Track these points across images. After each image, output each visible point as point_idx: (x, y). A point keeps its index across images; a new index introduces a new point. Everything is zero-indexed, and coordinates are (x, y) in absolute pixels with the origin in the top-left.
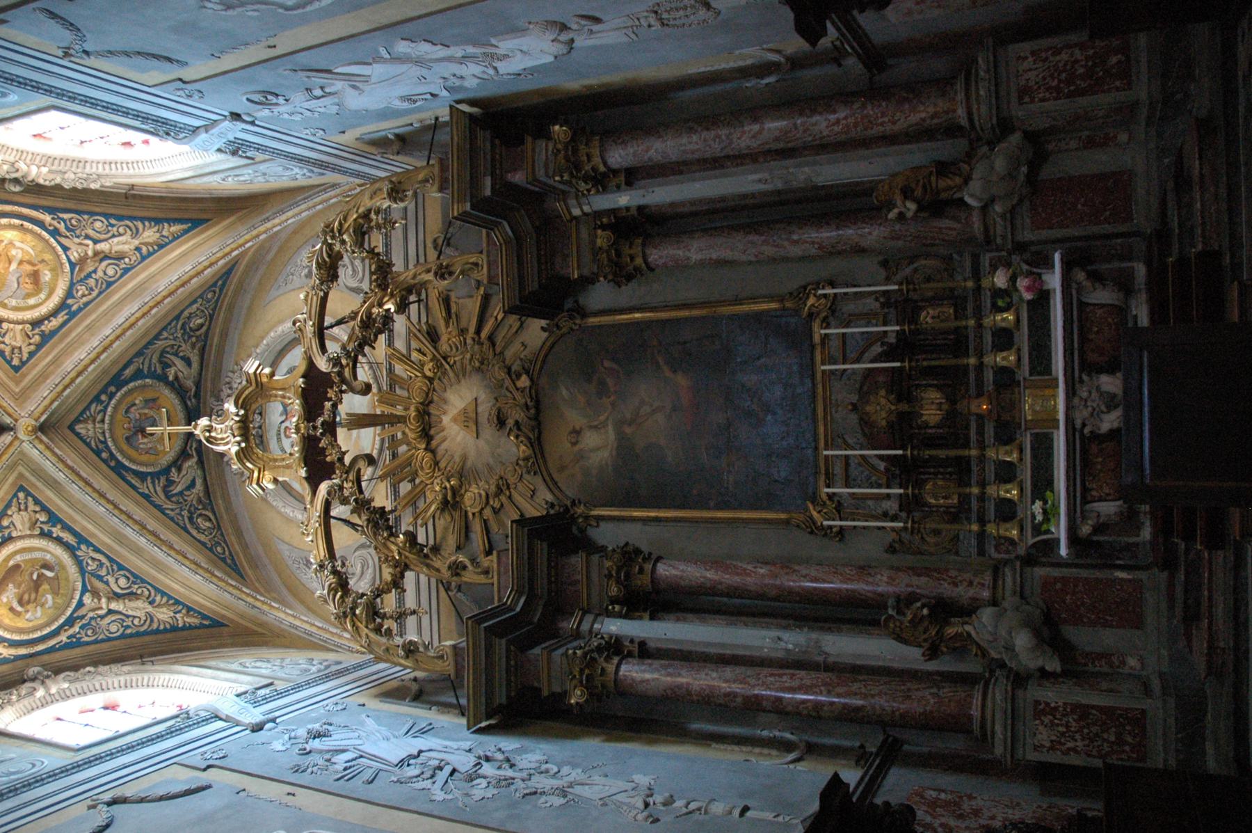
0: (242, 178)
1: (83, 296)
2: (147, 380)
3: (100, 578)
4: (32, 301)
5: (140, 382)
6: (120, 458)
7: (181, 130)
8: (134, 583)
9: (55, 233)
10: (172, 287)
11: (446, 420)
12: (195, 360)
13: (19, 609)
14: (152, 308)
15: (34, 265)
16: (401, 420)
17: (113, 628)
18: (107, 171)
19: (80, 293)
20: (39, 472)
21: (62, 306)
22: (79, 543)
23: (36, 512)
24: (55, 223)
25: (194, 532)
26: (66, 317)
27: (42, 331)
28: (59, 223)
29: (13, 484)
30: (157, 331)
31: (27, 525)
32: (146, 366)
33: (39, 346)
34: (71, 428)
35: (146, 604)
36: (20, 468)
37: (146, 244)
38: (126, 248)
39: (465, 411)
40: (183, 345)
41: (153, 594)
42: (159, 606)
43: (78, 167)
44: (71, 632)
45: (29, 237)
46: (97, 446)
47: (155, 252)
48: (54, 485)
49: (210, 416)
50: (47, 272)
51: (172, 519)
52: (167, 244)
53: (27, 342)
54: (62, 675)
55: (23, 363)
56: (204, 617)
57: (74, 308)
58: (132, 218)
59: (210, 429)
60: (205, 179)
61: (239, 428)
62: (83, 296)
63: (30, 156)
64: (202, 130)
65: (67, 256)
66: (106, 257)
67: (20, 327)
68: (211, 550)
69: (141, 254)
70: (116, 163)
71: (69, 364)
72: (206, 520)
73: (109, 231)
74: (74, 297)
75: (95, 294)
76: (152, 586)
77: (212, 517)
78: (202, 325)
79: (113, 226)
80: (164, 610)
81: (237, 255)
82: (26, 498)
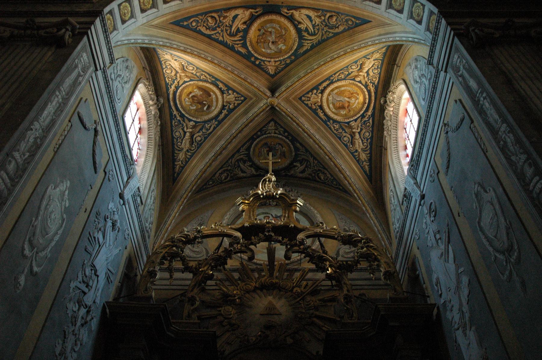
0: (392, 199)
1: (334, 127)
2: (294, 153)
3: (201, 129)
4: (331, 106)
5: (293, 150)
9: (363, 116)
10: (339, 166)
11: (270, 298)
12: (304, 175)
13: (191, 96)
14: (328, 156)
15: (348, 107)
16: (271, 275)
17: (177, 134)
18: (392, 139)
19: (335, 126)
22: (218, 121)
23: (234, 104)
24: (367, 116)
25: (220, 172)
26: (324, 119)
28: (368, 118)
29: (248, 96)
31: (228, 100)
32: (301, 153)
33: (310, 108)
34: (272, 120)
35: (187, 148)
36: (255, 98)
38: (357, 146)
39: (275, 308)
40: (311, 170)
41: (192, 152)
42: (186, 154)
43: (393, 126)
44: (177, 116)
45: (360, 106)
46: (263, 130)
47: (355, 158)
48: (246, 112)
49: (276, 182)
50: (345, 112)
51: (227, 161)
52: (359, 164)
54: (158, 112)
55: (303, 101)
56: (178, 174)
57: (328, 123)
59: (270, 181)
60: (391, 182)
61: (270, 195)
62: (334, 127)
63: (397, 108)
65: (352, 121)
66: (352, 137)
67: (319, 101)
68: (211, 179)
71: (302, 120)
73: (364, 139)
74: (333, 123)
75: (335, 132)
76: (195, 152)
78: (320, 179)
79: (367, 140)
80: (184, 156)
82: (241, 100)
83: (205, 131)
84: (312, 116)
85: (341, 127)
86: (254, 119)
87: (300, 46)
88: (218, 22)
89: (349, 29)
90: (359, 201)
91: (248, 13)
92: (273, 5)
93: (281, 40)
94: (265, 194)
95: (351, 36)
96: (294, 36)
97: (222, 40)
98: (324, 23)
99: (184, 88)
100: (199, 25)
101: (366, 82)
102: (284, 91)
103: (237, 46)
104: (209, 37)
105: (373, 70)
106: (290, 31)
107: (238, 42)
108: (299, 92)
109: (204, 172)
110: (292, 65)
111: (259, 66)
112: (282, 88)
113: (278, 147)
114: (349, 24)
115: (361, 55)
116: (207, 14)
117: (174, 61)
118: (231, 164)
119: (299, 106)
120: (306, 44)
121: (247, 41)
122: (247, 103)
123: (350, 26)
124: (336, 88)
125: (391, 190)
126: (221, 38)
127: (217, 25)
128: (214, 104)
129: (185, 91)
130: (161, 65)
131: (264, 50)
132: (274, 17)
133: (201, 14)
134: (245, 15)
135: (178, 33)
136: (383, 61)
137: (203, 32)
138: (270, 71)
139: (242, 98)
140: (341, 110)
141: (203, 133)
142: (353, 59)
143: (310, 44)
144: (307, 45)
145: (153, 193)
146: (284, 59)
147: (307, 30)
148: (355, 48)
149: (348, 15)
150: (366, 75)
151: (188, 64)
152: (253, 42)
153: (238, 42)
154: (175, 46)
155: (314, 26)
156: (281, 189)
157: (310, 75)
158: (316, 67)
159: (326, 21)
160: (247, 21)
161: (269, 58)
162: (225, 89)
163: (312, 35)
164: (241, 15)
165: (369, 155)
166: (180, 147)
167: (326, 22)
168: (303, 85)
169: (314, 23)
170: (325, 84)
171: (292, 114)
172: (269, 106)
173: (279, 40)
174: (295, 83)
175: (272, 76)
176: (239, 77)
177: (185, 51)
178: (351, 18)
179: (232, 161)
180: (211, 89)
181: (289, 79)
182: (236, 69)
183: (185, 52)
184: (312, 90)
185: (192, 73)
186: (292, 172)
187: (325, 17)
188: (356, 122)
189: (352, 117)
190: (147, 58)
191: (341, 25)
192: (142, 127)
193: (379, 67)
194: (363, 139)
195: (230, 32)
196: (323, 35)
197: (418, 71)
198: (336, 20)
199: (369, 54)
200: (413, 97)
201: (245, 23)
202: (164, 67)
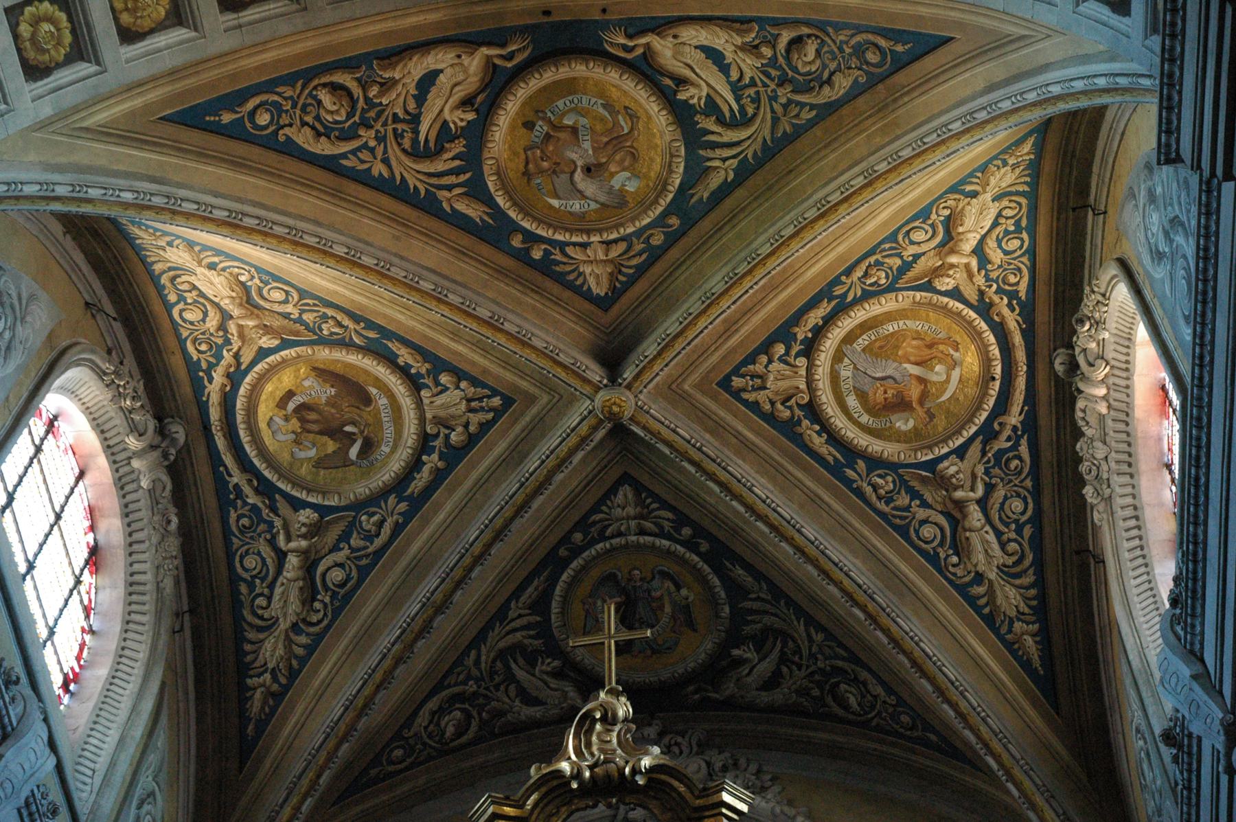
0: (1145, 766)
1: (875, 488)
2: (727, 609)
3: (345, 537)
4: (852, 401)
5: (723, 594)
6: (574, 565)
7: (1190, 629)
8: (334, 595)
9: (988, 433)
10: (909, 644)
12: (777, 696)
13: (291, 406)
14: (864, 609)
15: (921, 402)
17: (250, 562)
18: (1120, 513)
19: (880, 481)
20: (538, 428)
21: (851, 453)
22: (410, 499)
23: (466, 426)
24: (1007, 432)
25: (432, 704)
26: (830, 459)
27: (799, 422)
28: (1009, 439)
29: (516, 388)
30: (824, 621)
31: (442, 413)
32: (756, 605)
33: (770, 418)
34: (625, 479)
35: (292, 618)
36: (545, 398)
37: (991, 592)
40: (803, 673)
41: (312, 630)
42: (289, 642)
43: (1118, 462)
44: (247, 489)
45: (972, 391)
46: (594, 523)
47: (978, 610)
48: (517, 454)
49: (633, 721)
50: (911, 424)
51: (459, 662)
52: (996, 631)
53: (775, 398)
54: (166, 479)
55: (736, 394)
56: (262, 725)
57: (850, 473)
58: (1039, 564)
59: (609, 719)
60: (1132, 693)
61: (608, 776)
62: (875, 488)
63: (1123, 383)
64: (1198, 668)
65: (946, 456)
66: (955, 523)
67: (803, 386)
68: (398, 736)
69: (970, 584)
70: (1139, 528)
71: (741, 468)
72: (457, 727)
73: (1007, 525)
74: (870, 470)
75: (882, 506)
76: (328, 627)
77: (464, 739)
78: (846, 707)
79: (1019, 531)
80: (280, 651)
81: (989, 767)
82: (491, 410)
83: (362, 543)
84: (783, 451)
85: (903, 483)
86: (548, 479)
87: (696, 172)
88: (361, 103)
89: (875, 81)
90: (1010, 786)
91: (474, 63)
92: (571, 23)
93: (618, 157)
94: (587, 774)
95: (882, 109)
96: (668, 138)
97: (386, 175)
98: (774, 73)
99: (263, 378)
100: (285, 120)
101: (981, 293)
102: (655, 358)
103: (446, 194)
104: (329, 164)
105: (999, 241)
106: (649, 118)
107: (452, 180)
108: (714, 358)
109: (366, 706)
110: (674, 253)
111: (545, 267)
112: (645, 345)
113: (661, 588)
114: (868, 63)
115: (937, 183)
116: (311, 80)
117: (206, 272)
118: (475, 672)
119: (722, 413)
120: (717, 163)
121: (486, 170)
122: (516, 421)
123: (872, 69)
124: (864, 327)
125: (1138, 731)
126: (379, 169)
127: (356, 118)
128: (388, 431)
129: (269, 388)
130: (160, 289)
131: (555, 203)
132: (579, 69)
133: (290, 80)
134: (465, 71)
135: (200, 154)
136: (1033, 196)
137: (306, 146)
138: (592, 282)
139: (496, 401)
140: (893, 418)
141: (353, 550)
142: (911, 204)
143: (734, 163)
144: (722, 169)
145: (146, 808)
146: (639, 233)
147: (712, 107)
148: (906, 153)
149: (859, 30)
150: (974, 263)
151: (264, 277)
152: (511, 174)
153: (452, 180)
154: (189, 207)
155: (737, 88)
156: (656, 750)
157: (747, 283)
158: (766, 249)
159: (781, 60)
160: (475, 97)
161: (582, 231)
162: (423, 371)
163: (733, 124)
164: (449, 71)
165: (1033, 592)
166: (266, 616)
167: (780, 68)
168: (730, 327)
169: (734, 75)
170: (815, 317)
171: (699, 449)
172: (601, 422)
173: (610, 157)
174: (693, 323)
175: (603, 303)
176: (469, 315)
177: (232, 226)
178: (871, 37)
179: (479, 656)
180: (366, 372)
181: (670, 305)
182: (453, 286)
183: (237, 226)
184: (765, 348)
185: (286, 316)
186: (730, 688)
187: (774, 47)
188: (962, 458)
189: (945, 441)
190: (97, 265)
191: (838, 69)
192: (101, 541)
193: (1024, 223)
194: (1002, 528)
195: (415, 141)
196: (775, 121)
197: (1157, 208)
198: (818, 52)
199: (971, 175)
200: (1159, 320)
201: (467, 102)
202: (172, 298)
